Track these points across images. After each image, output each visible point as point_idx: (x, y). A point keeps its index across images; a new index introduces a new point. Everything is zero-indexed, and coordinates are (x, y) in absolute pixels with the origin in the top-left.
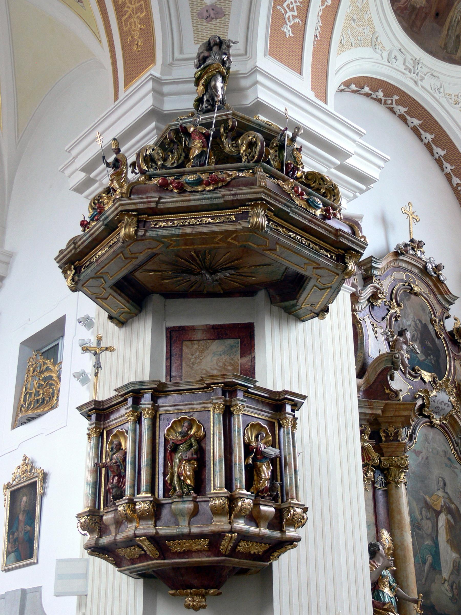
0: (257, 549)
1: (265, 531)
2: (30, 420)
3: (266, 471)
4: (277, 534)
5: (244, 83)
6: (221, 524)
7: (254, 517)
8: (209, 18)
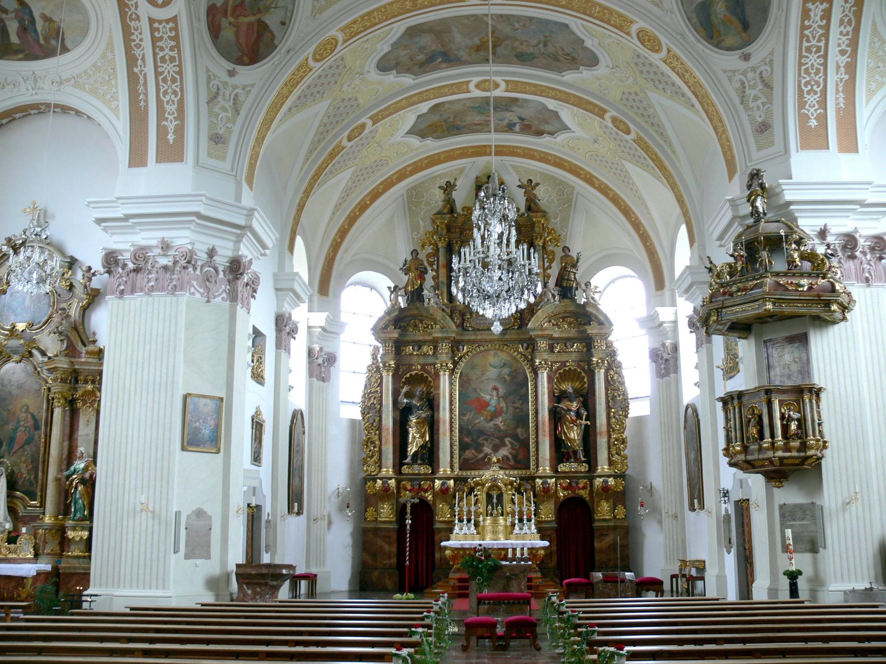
0: (797, 462)
1: (795, 454)
2: (731, 378)
3: (793, 426)
4: (802, 454)
5: (777, 190)
6: (770, 454)
7: (787, 449)
8: (762, 132)
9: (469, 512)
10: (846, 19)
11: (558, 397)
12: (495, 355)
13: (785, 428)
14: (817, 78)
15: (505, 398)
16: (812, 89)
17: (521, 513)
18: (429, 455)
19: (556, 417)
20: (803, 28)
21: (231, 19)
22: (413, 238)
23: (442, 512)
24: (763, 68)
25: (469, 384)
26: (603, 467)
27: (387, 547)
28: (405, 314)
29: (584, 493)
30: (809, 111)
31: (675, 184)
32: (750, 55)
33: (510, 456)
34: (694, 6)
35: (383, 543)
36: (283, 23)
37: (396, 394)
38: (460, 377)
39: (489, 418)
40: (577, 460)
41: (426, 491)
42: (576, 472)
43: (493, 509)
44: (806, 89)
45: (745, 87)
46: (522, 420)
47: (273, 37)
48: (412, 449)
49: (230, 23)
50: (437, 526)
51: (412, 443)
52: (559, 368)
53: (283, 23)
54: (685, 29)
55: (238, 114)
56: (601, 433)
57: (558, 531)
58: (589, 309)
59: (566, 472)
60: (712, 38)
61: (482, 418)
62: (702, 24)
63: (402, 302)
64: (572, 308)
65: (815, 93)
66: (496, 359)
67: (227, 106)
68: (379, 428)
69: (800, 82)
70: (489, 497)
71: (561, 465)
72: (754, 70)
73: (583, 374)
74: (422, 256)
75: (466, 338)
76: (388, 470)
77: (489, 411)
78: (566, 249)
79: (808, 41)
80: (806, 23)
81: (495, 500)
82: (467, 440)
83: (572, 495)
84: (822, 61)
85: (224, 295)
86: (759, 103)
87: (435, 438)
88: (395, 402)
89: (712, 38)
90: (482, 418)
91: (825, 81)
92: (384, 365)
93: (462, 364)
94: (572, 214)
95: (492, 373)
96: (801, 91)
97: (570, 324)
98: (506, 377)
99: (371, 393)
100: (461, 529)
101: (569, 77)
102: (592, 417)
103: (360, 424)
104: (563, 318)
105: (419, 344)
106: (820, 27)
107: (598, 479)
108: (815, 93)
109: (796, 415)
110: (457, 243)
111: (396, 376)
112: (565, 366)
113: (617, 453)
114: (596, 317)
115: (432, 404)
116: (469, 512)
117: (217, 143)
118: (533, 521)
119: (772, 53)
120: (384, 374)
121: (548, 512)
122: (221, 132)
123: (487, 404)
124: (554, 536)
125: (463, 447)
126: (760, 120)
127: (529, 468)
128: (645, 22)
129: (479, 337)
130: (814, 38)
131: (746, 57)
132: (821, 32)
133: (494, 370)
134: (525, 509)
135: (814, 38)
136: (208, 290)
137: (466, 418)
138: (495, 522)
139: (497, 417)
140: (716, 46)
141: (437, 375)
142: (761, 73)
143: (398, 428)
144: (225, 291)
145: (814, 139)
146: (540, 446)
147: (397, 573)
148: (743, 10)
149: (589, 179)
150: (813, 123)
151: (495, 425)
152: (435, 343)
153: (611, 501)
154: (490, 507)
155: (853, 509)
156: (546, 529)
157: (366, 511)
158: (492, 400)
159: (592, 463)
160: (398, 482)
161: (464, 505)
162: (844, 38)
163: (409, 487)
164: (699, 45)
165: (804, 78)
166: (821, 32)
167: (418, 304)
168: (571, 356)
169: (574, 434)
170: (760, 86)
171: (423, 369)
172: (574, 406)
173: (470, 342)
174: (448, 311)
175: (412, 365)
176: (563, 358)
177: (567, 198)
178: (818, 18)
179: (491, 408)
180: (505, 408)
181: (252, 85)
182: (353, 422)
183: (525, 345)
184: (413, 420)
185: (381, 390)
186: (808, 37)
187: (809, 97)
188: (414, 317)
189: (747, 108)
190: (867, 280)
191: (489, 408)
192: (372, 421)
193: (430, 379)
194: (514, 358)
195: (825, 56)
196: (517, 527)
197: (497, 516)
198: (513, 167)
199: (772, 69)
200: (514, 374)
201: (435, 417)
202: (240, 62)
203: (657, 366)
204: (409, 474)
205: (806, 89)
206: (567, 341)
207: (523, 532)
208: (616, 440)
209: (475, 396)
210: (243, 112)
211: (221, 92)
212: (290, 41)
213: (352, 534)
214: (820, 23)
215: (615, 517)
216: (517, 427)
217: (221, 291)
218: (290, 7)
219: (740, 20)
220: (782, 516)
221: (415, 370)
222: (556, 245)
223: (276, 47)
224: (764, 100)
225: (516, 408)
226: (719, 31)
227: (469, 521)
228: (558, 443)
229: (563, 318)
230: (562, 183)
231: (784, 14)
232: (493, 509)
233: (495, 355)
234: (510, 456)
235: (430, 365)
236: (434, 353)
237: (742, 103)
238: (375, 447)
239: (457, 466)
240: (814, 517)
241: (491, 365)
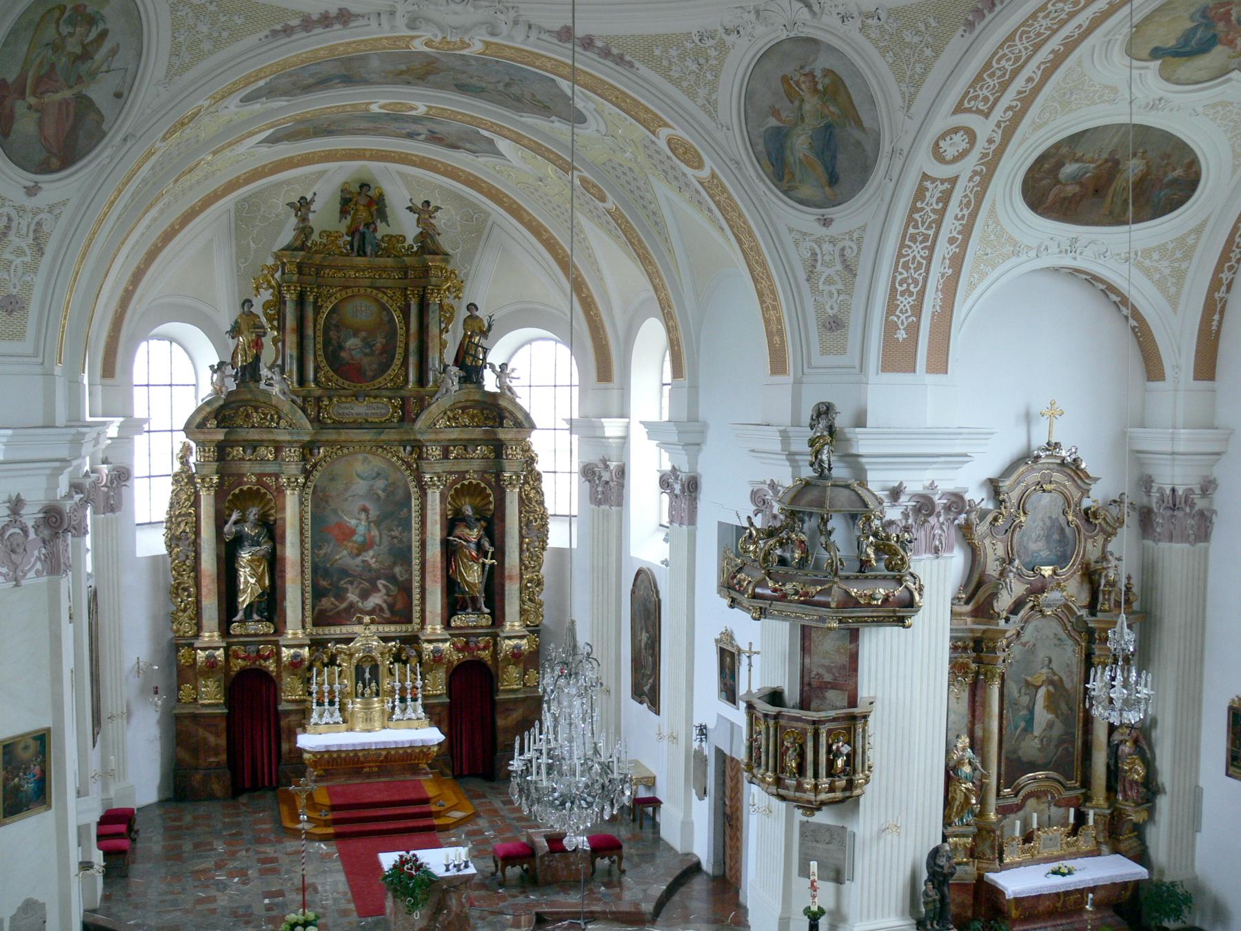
3: (840, 763)
7: (832, 789)
9: (331, 692)
10: (965, 201)
11: (452, 523)
12: (365, 459)
13: (831, 764)
14: (916, 276)
16: (908, 289)
17: (403, 690)
18: (270, 605)
19: (450, 551)
20: (914, 209)
21: (32, 100)
22: (239, 268)
23: (291, 690)
24: (847, 243)
25: (327, 502)
26: (513, 624)
27: (212, 739)
28: (233, 399)
29: (485, 655)
30: (899, 317)
31: (676, 328)
32: (832, 220)
33: (384, 606)
34: (763, 129)
35: (207, 735)
36: (118, 95)
38: (314, 493)
39: (355, 551)
40: (477, 610)
41: (267, 658)
42: (475, 627)
43: (364, 687)
44: (900, 289)
45: (816, 260)
46: (402, 555)
47: (102, 118)
48: (244, 600)
49: (30, 107)
50: (283, 707)
51: (245, 591)
52: (455, 482)
53: (118, 95)
54: (744, 157)
55: (43, 254)
56: (511, 578)
57: (451, 707)
58: (503, 403)
59: (461, 628)
60: (781, 180)
61: (345, 552)
62: (769, 154)
63: (232, 385)
64: (477, 397)
65: (911, 294)
67: (24, 245)
68: (196, 567)
69: (894, 278)
70: (359, 670)
71: (455, 618)
72: (833, 241)
73: (489, 491)
74: (257, 309)
75: (324, 438)
76: (210, 635)
78: (472, 307)
79: (916, 227)
80: (919, 205)
81: (367, 676)
82: (324, 583)
83: (470, 659)
84: (926, 253)
85: (39, 566)
86: (833, 289)
87: (279, 583)
89: (781, 180)
90: (345, 552)
91: (925, 280)
93: (317, 474)
94: (482, 244)
95: (360, 486)
96: (893, 290)
97: (473, 417)
98: (380, 492)
99: (180, 515)
100: (321, 716)
101: (530, 120)
102: (500, 554)
103: (165, 562)
104: (464, 409)
105: (254, 446)
106: (934, 211)
107: (507, 642)
108: (911, 294)
109: (846, 749)
110: (311, 292)
111: (220, 493)
112: (465, 479)
113: (530, 600)
114: (511, 413)
115: (271, 530)
116: (331, 692)
117: (10, 313)
118: (420, 701)
119: (863, 228)
120: (203, 493)
121: (438, 684)
122: (14, 292)
124: (445, 714)
125: (318, 593)
126: (831, 312)
127: (410, 621)
128: (683, 129)
129: (343, 438)
130: (923, 223)
131: (826, 222)
132: (933, 217)
133: (361, 482)
134: (408, 684)
135: (923, 223)
136: (15, 567)
138: (367, 707)
140: (785, 192)
141: (280, 491)
142: (843, 249)
144: (39, 558)
145: (898, 358)
146: (428, 596)
147: (228, 774)
148: (834, 157)
149: (515, 211)
150: (901, 335)
152: (278, 447)
153: (521, 665)
154: (360, 684)
155: (889, 837)
156: (434, 706)
157: (179, 689)
158: (360, 526)
159: (497, 613)
160: (227, 649)
161: (322, 681)
162: (957, 223)
163: (242, 654)
164: (761, 185)
165: (901, 274)
166: (933, 217)
167: (252, 385)
168: (473, 466)
169: (473, 576)
170: (839, 267)
171: (259, 482)
172: (474, 534)
173: (331, 444)
174: (299, 401)
175: (244, 475)
176: (463, 466)
177: (477, 228)
178: (934, 200)
179: (358, 538)
180: (377, 539)
181: (64, 203)
182: (155, 559)
183: (408, 448)
184: (245, 555)
186: (916, 221)
187: (902, 299)
188: (245, 403)
189: (814, 290)
190: (937, 550)
193: (269, 496)
194: (393, 464)
195: (932, 249)
196: (397, 710)
197: (371, 697)
198: (399, 173)
199: (859, 249)
200: (390, 490)
201: (278, 552)
202: (44, 168)
203: (592, 487)
204: (241, 635)
205: (900, 289)
206: (466, 444)
207: (407, 716)
208: (530, 581)
210: (49, 250)
211: (14, 224)
212: (128, 124)
213: (159, 722)
214: (935, 206)
215: (524, 685)
216: (395, 564)
217: (33, 560)
218: (131, 67)
219: (826, 168)
220: (803, 835)
221: (246, 483)
222: (457, 297)
223: (104, 135)
224: (842, 287)
225: (394, 537)
226: (793, 175)
227: (332, 703)
228: (451, 586)
229: (464, 409)
230: (473, 205)
231: (891, 185)
232: (364, 687)
233: (365, 459)
234: (384, 606)
235: (270, 475)
236: (276, 458)
237: (808, 280)
240: (842, 844)
241: (359, 476)
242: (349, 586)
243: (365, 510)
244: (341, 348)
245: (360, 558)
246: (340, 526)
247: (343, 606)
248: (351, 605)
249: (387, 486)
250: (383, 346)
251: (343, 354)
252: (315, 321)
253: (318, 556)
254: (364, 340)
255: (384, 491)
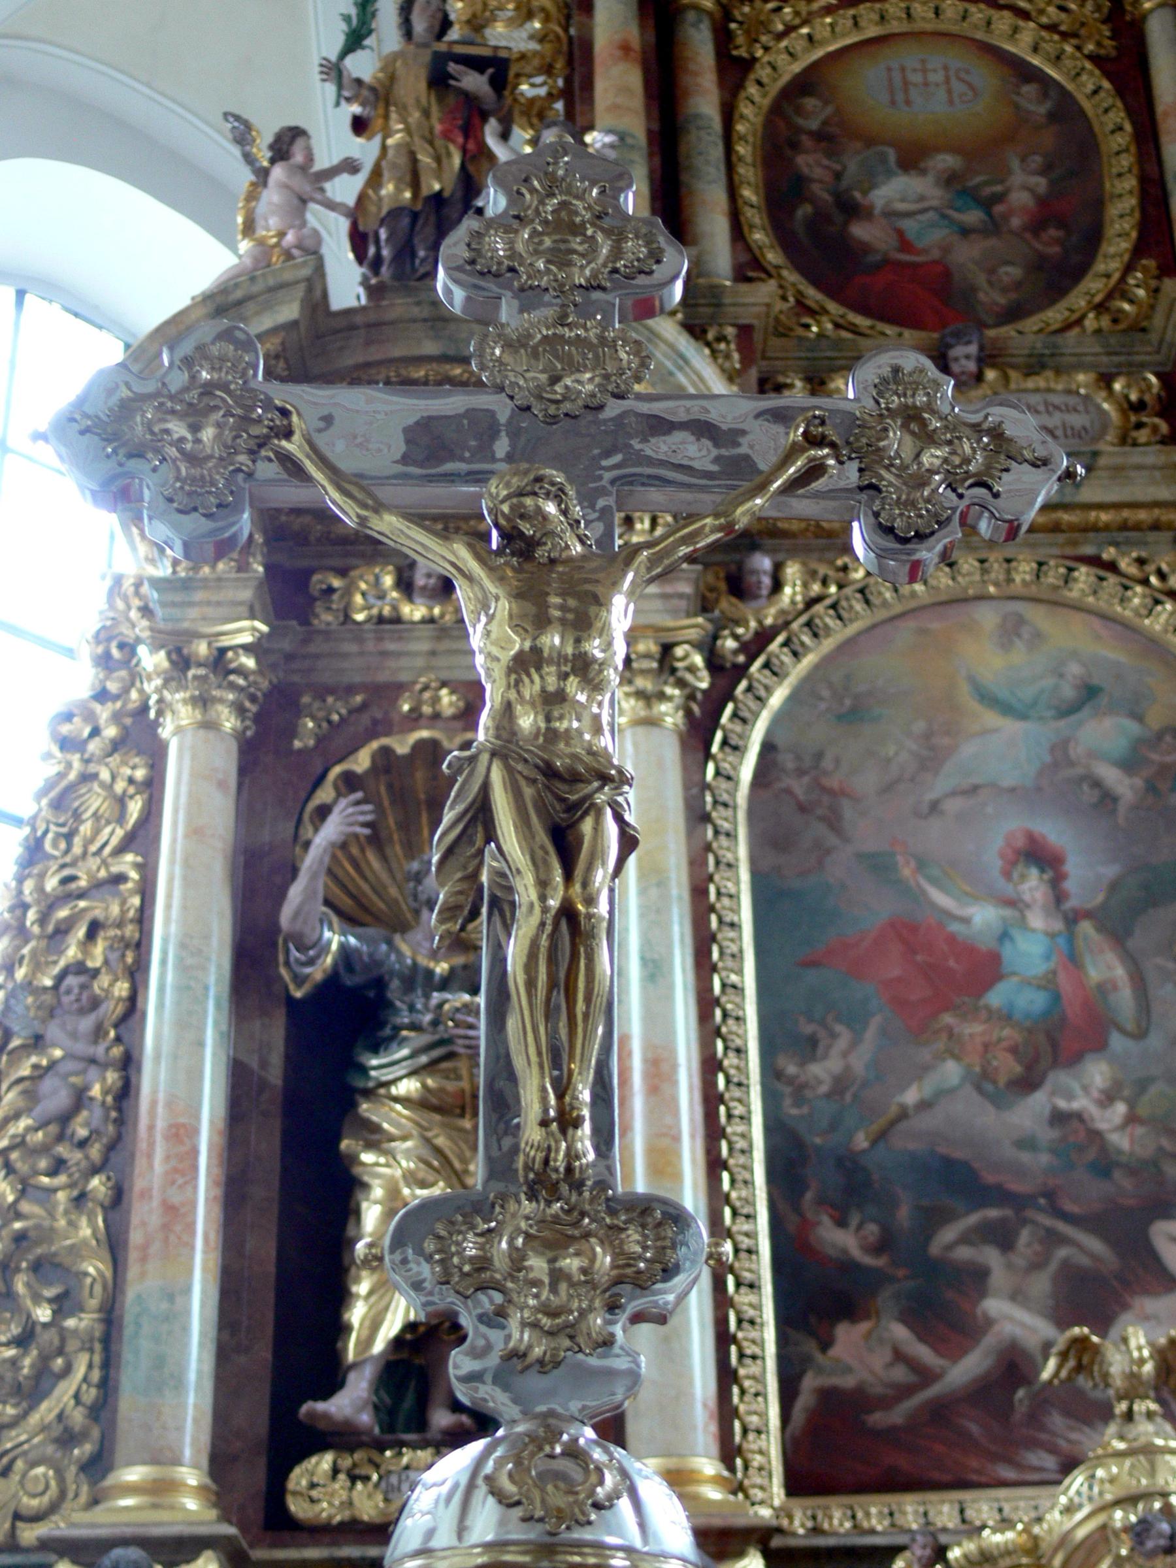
12: (1011, 630)
15: (1118, 920)
25: (834, 822)
37: (258, 879)
39: (1008, 1066)
61: (951, 1071)
66: (1019, 655)
77: (1005, 1017)
82: (842, 1240)
88: (255, 953)
90: (951, 1071)
92: (181, 662)
95: (1003, 748)
98: (1111, 776)
99: (68, 892)
123: (985, 968)
125: (815, 1298)
133: (1010, 726)
137: (822, 1071)
139: (1074, 1059)
143: (268, 1143)
151: (1059, 1118)
179: (1016, 997)
180: (1124, 999)
185: (148, 872)
191: (996, 997)
192: (56, 1097)
209: (873, 910)
221: (415, 719)
233: (1011, 630)
238: (63, 1304)
239: (769, 1450)
242: (991, 1257)
243: (1038, 855)
244: (851, 209)
245: (1039, 1101)
246: (913, 935)
247: (966, 1369)
248: (1014, 1367)
249: (1138, 744)
250: (1043, 202)
251: (860, 231)
252: (729, 115)
253: (800, 1090)
254: (950, 180)
255: (1129, 765)
